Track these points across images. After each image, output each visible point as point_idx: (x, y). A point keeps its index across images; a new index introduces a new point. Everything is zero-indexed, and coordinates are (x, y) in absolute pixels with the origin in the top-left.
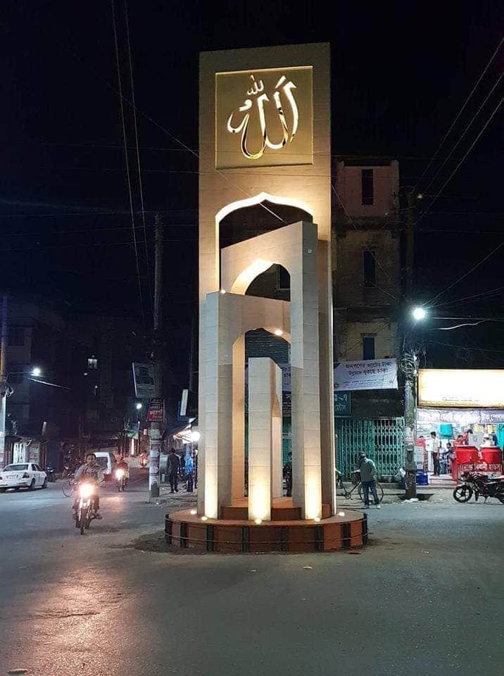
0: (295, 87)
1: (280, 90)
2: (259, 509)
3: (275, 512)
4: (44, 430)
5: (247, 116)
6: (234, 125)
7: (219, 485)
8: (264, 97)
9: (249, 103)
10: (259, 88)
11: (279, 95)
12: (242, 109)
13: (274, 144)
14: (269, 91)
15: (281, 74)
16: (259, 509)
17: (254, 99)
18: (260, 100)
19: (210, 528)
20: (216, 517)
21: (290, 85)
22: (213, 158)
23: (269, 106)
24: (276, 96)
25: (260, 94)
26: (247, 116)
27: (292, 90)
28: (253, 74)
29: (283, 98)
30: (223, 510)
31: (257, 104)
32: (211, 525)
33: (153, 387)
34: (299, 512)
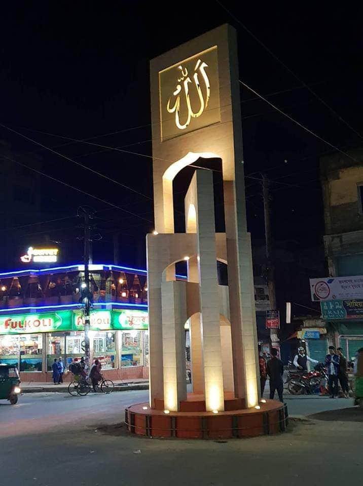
0: (207, 66)
1: (198, 71)
2: (215, 402)
3: (228, 404)
4: (339, 382)
5: (178, 99)
6: (171, 108)
7: (178, 383)
8: (188, 79)
9: (179, 88)
10: (185, 74)
11: (198, 76)
12: (175, 93)
13: (180, 123)
14: (191, 76)
15: (196, 59)
16: (215, 402)
17: (182, 84)
18: (186, 83)
19: (173, 419)
20: (177, 411)
21: (204, 65)
22: (160, 133)
23: (192, 86)
24: (195, 76)
25: (185, 78)
26: (178, 99)
27: (205, 68)
28: (181, 65)
29: (200, 78)
30: (183, 403)
31: (194, 79)
32: (174, 417)
33: (269, 302)
34: (243, 401)
